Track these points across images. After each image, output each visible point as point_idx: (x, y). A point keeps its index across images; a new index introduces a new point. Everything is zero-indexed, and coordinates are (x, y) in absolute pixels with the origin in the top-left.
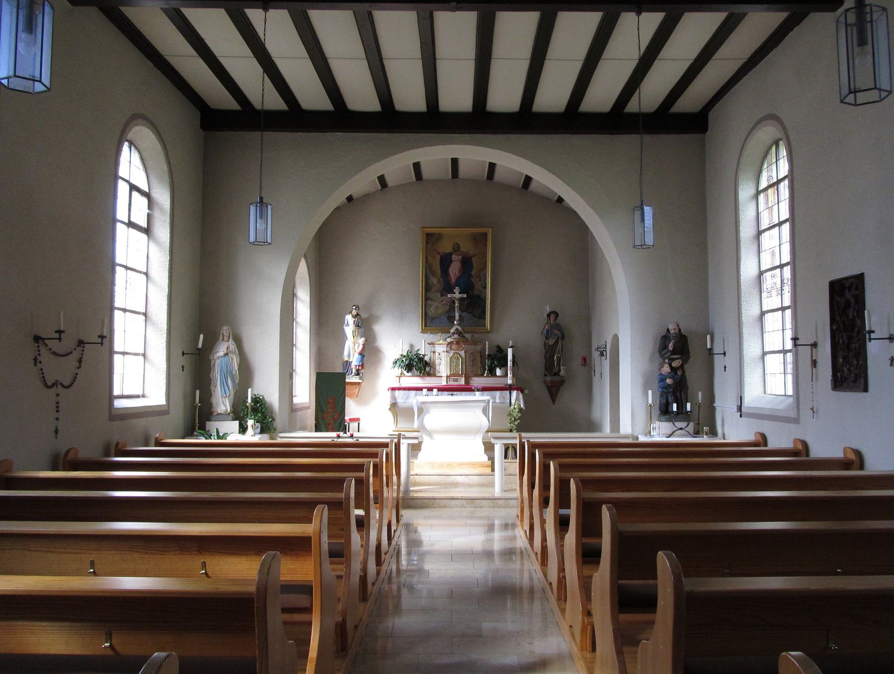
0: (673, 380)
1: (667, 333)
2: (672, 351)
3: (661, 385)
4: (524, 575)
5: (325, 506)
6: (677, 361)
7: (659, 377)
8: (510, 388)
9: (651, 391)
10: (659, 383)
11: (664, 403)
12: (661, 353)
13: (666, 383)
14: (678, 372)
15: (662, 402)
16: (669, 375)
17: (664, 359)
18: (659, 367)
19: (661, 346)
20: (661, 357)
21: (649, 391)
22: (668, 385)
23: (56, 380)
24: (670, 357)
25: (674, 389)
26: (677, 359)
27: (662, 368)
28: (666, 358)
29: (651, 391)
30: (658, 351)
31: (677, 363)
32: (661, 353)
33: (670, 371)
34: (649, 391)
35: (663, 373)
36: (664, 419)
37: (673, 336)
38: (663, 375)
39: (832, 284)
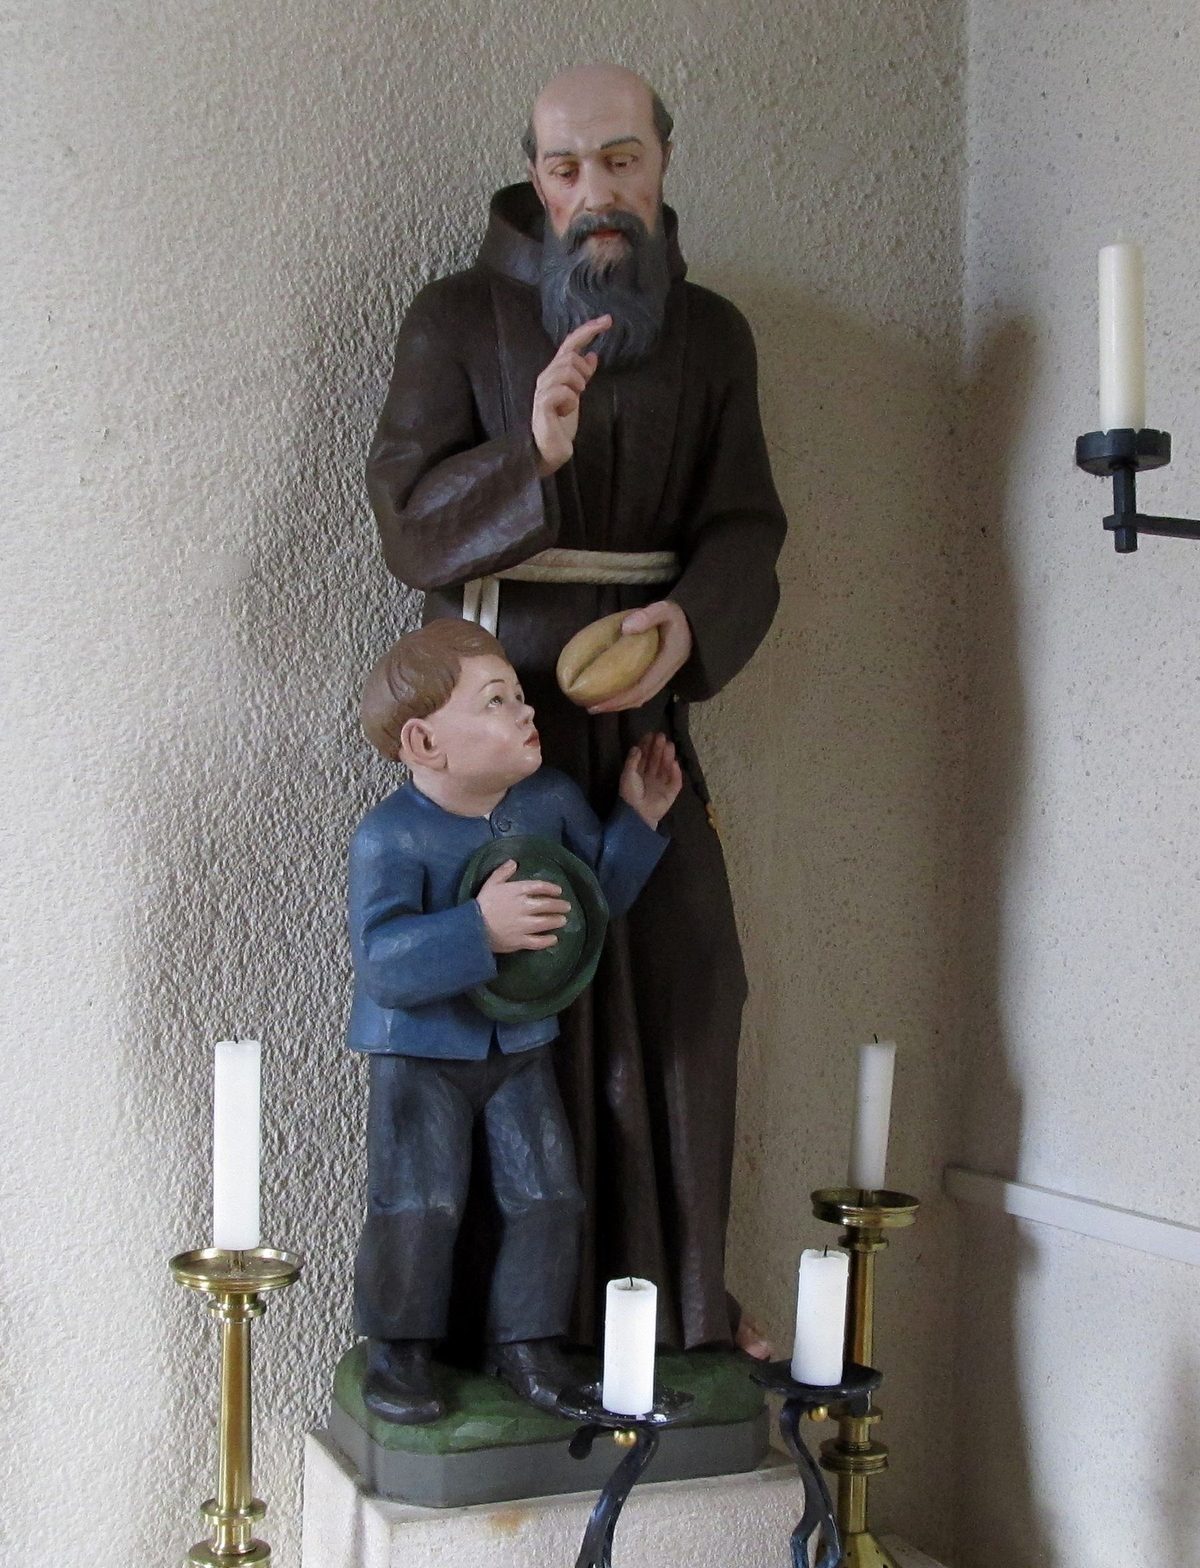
0: (578, 891)
1: (493, 240)
2: (562, 473)
3: (396, 963)
4: (520, 1136)
5: (573, 682)
6: (637, 620)
7: (369, 847)
8: (409, 590)
9: (251, 1051)
10: (381, 923)
11: (433, 1216)
12: (404, 499)
13: (476, 928)
14: (633, 785)
15: (408, 1203)
16: (511, 833)
17: (453, 593)
18: (382, 702)
19: (411, 415)
20: (396, 562)
21: (224, 1052)
22: (508, 960)
23: (1106, 528)
24: (521, 572)
25: (566, 1019)
26: (643, 595)
27: (426, 706)
28: (481, 570)
29: (251, 1051)
30: (377, 470)
31: (632, 655)
32: (404, 499)
33: (532, 758)
34: (224, 1052)
35: (428, 784)
36: (432, 1466)
37: (581, 278)
38: (433, 813)
39: (1166, 437)
